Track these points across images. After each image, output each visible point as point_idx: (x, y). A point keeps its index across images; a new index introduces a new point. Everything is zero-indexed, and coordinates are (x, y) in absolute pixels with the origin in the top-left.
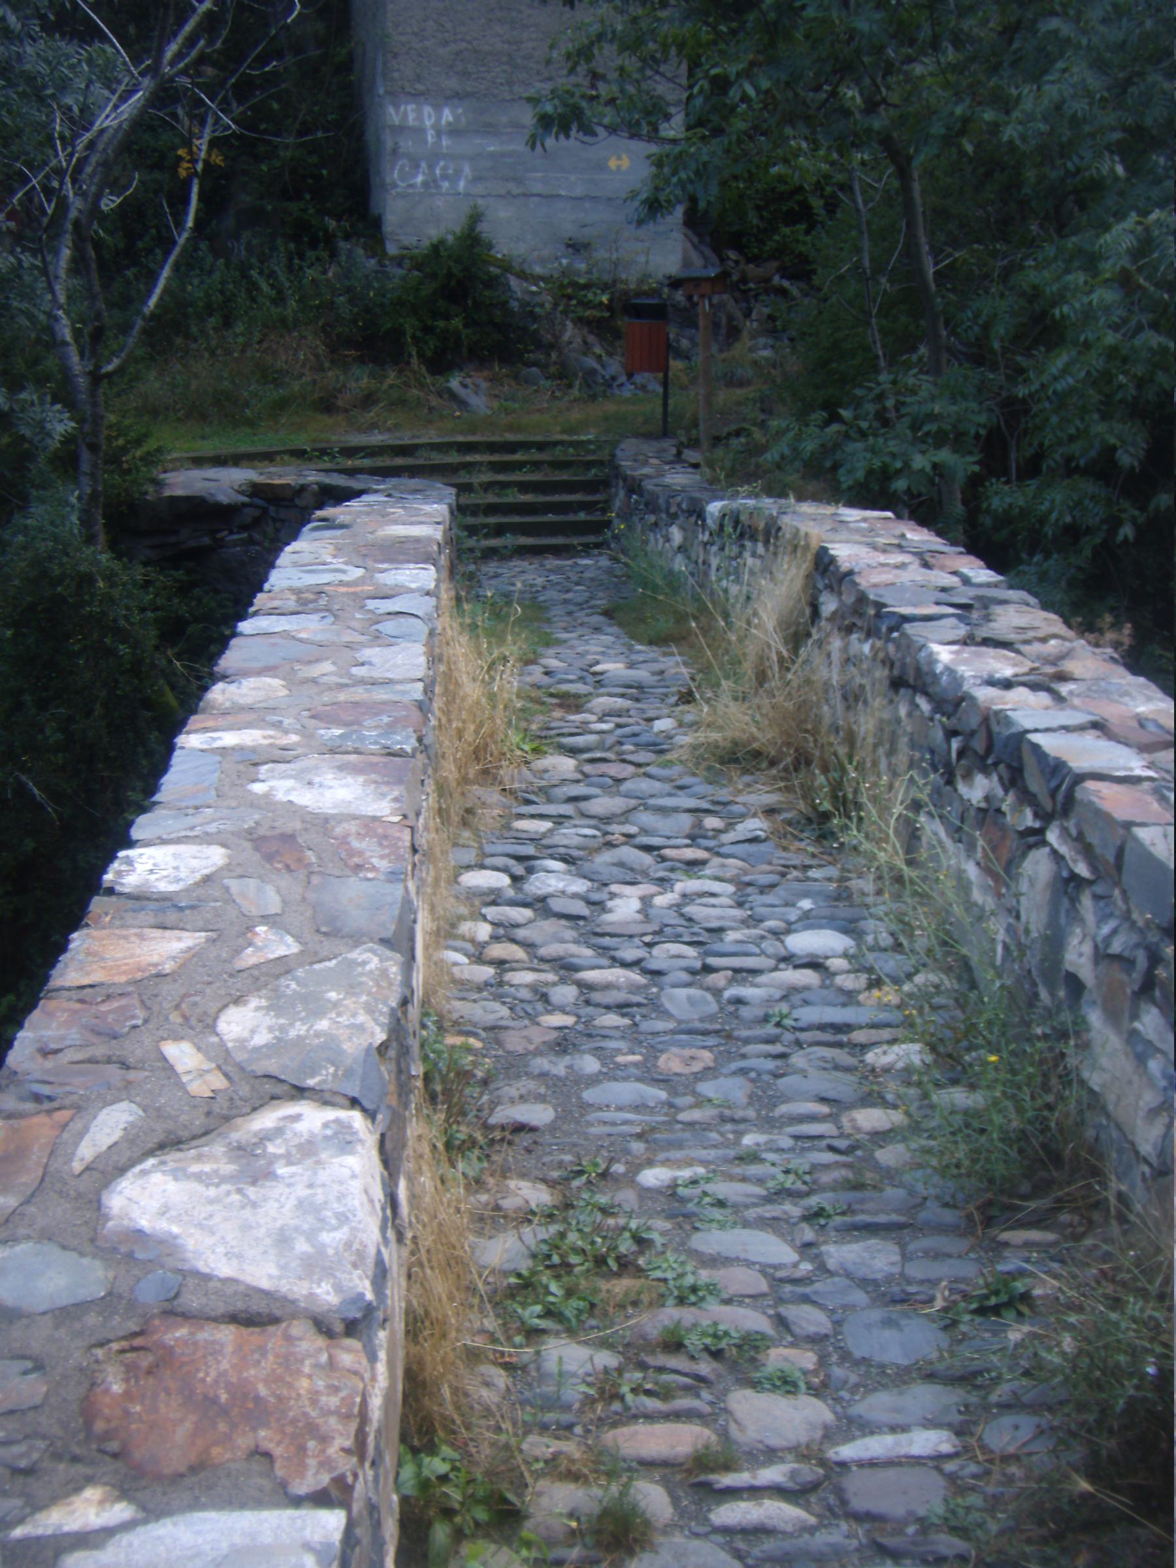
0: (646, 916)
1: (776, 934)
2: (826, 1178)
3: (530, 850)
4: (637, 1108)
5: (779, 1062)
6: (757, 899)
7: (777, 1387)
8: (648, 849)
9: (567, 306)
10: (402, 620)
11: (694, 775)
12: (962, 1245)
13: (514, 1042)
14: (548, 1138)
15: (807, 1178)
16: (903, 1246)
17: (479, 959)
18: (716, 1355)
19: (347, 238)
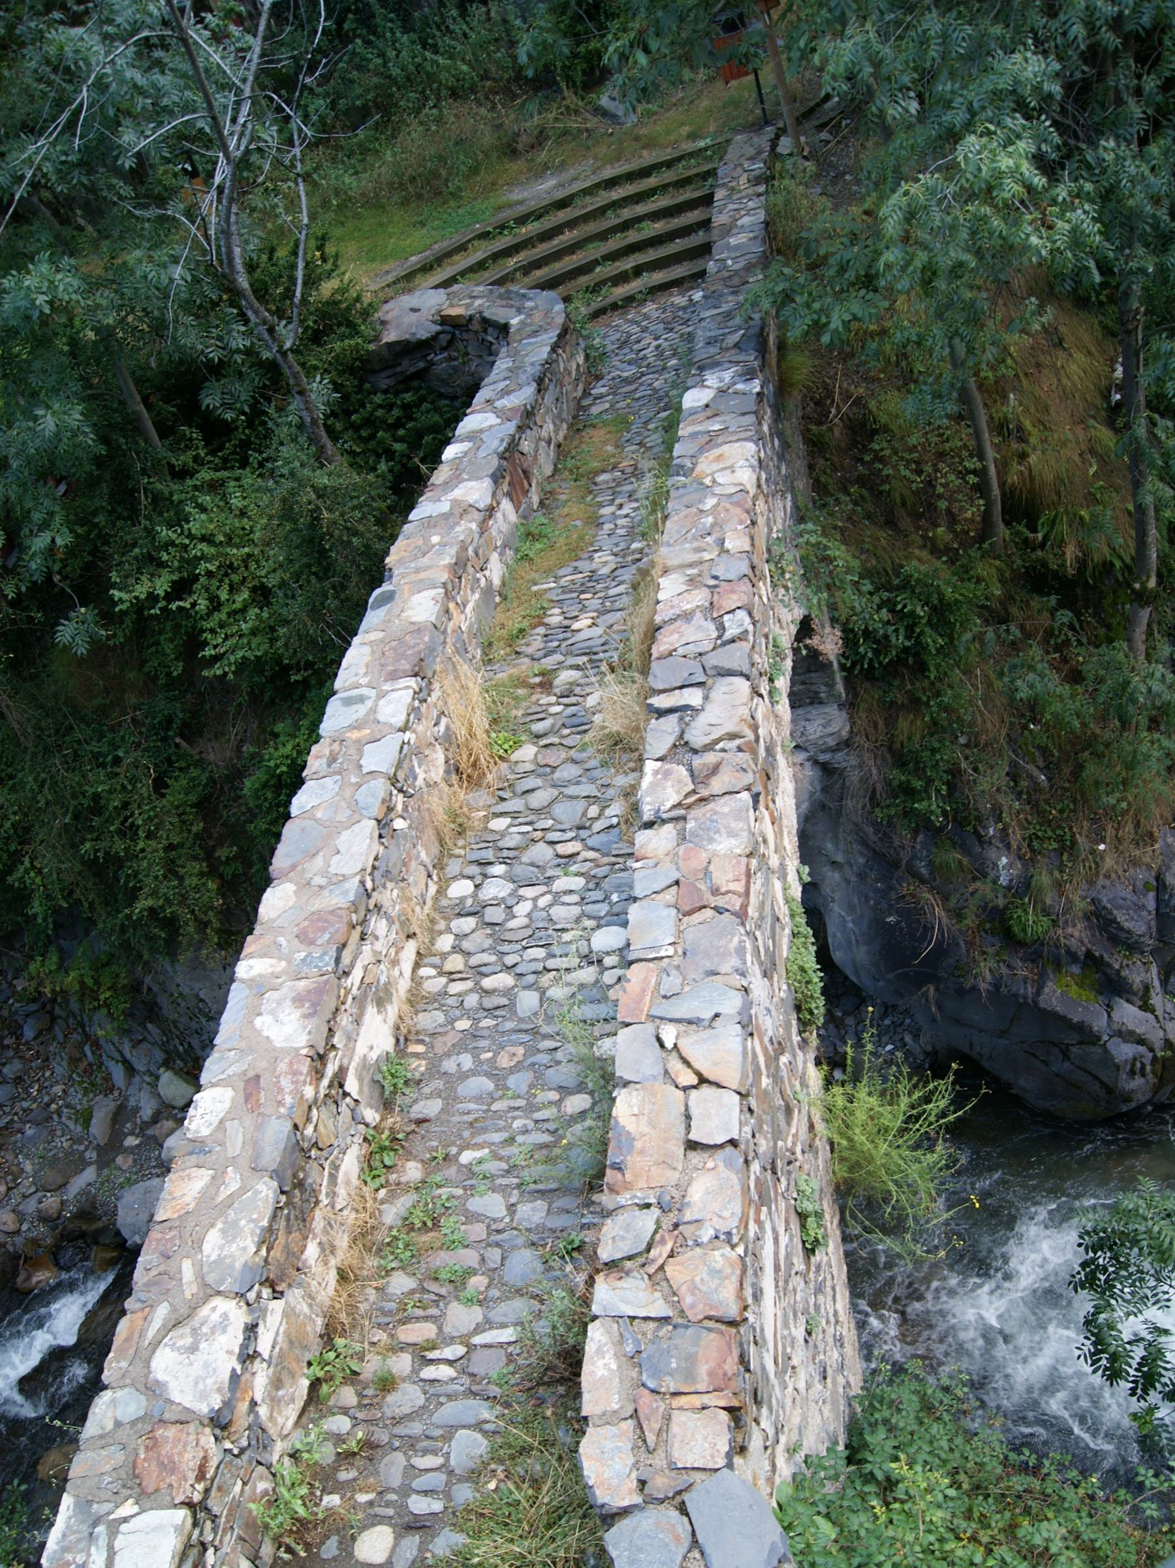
14: (433, 1128)
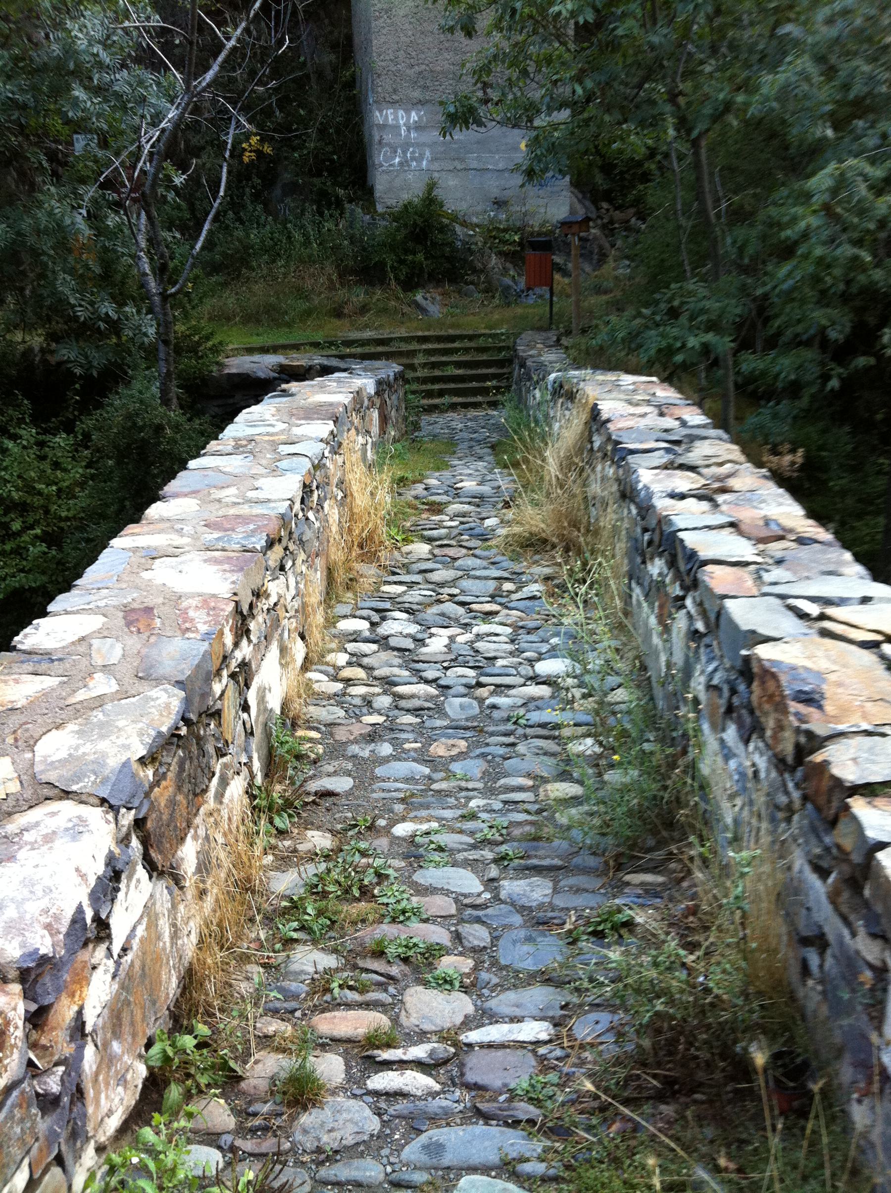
0: (450, 649)
1: (531, 662)
2: (517, 832)
3: (388, 605)
4: (407, 780)
5: (507, 750)
6: (525, 637)
7: (440, 985)
8: (462, 604)
9: (493, 243)
10: (295, 458)
11: (503, 555)
12: (597, 883)
13: (341, 734)
14: (344, 801)
15: (504, 832)
16: (556, 883)
17: (335, 679)
18: (406, 960)
19: (350, 201)
